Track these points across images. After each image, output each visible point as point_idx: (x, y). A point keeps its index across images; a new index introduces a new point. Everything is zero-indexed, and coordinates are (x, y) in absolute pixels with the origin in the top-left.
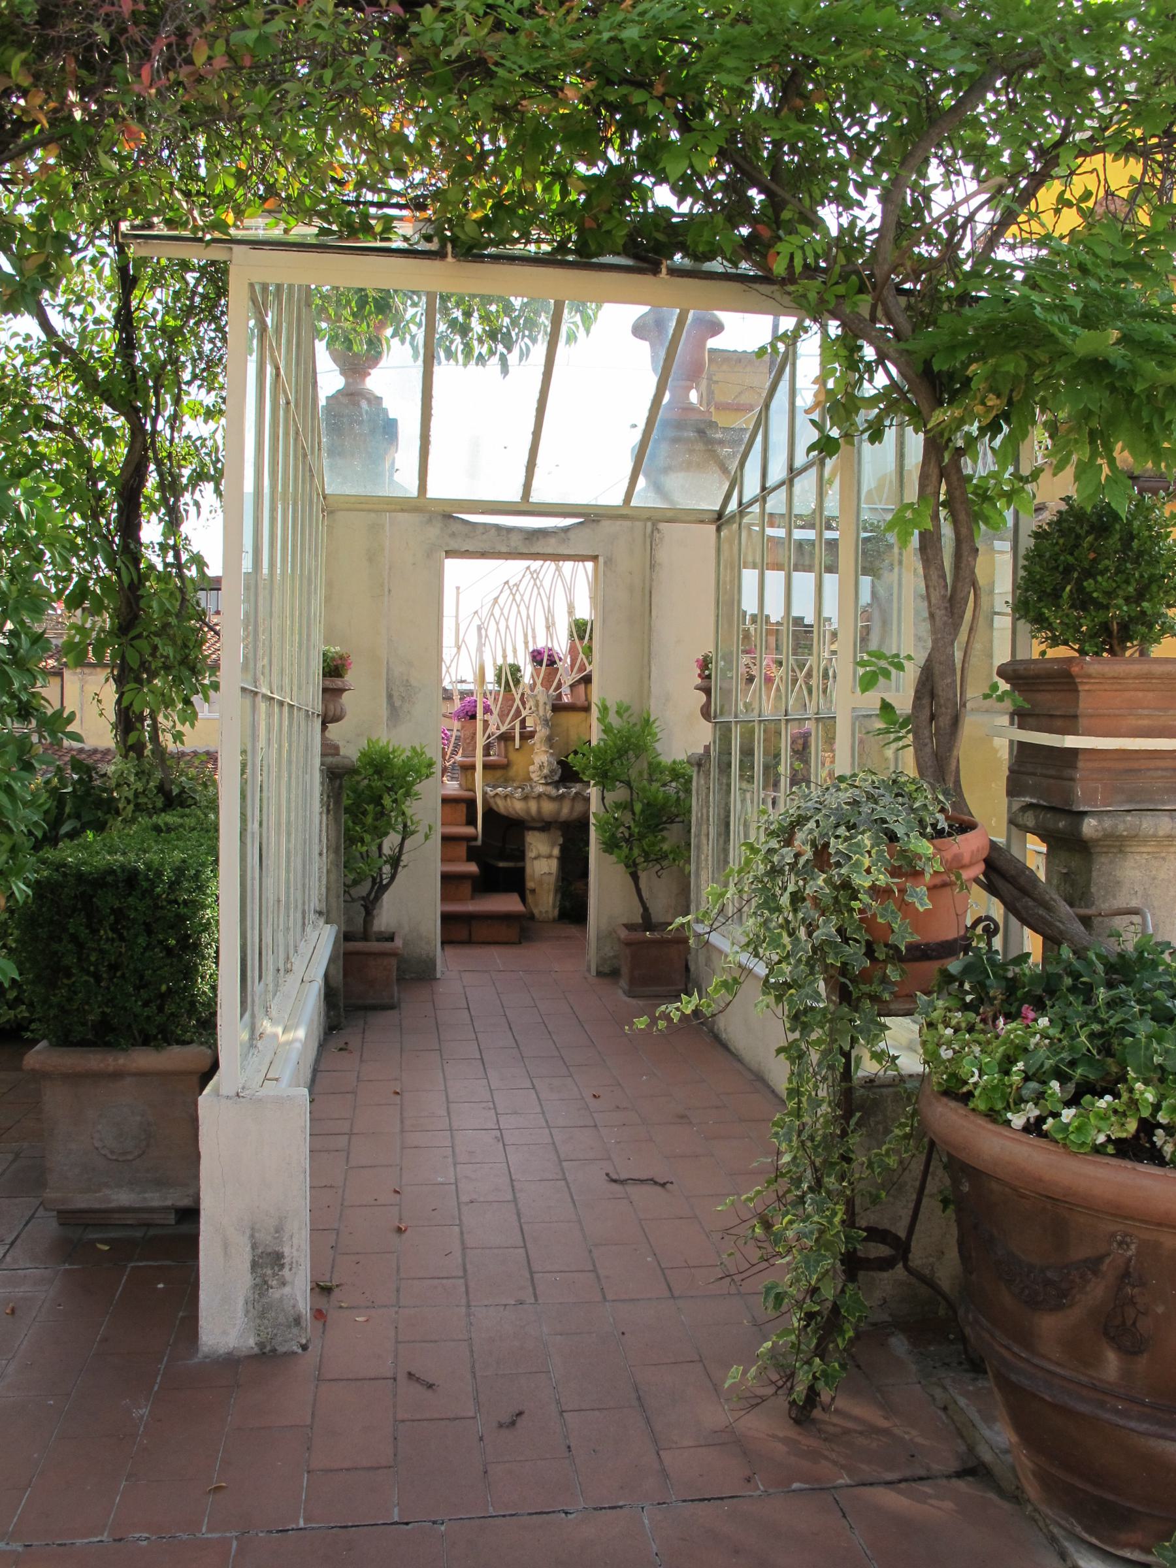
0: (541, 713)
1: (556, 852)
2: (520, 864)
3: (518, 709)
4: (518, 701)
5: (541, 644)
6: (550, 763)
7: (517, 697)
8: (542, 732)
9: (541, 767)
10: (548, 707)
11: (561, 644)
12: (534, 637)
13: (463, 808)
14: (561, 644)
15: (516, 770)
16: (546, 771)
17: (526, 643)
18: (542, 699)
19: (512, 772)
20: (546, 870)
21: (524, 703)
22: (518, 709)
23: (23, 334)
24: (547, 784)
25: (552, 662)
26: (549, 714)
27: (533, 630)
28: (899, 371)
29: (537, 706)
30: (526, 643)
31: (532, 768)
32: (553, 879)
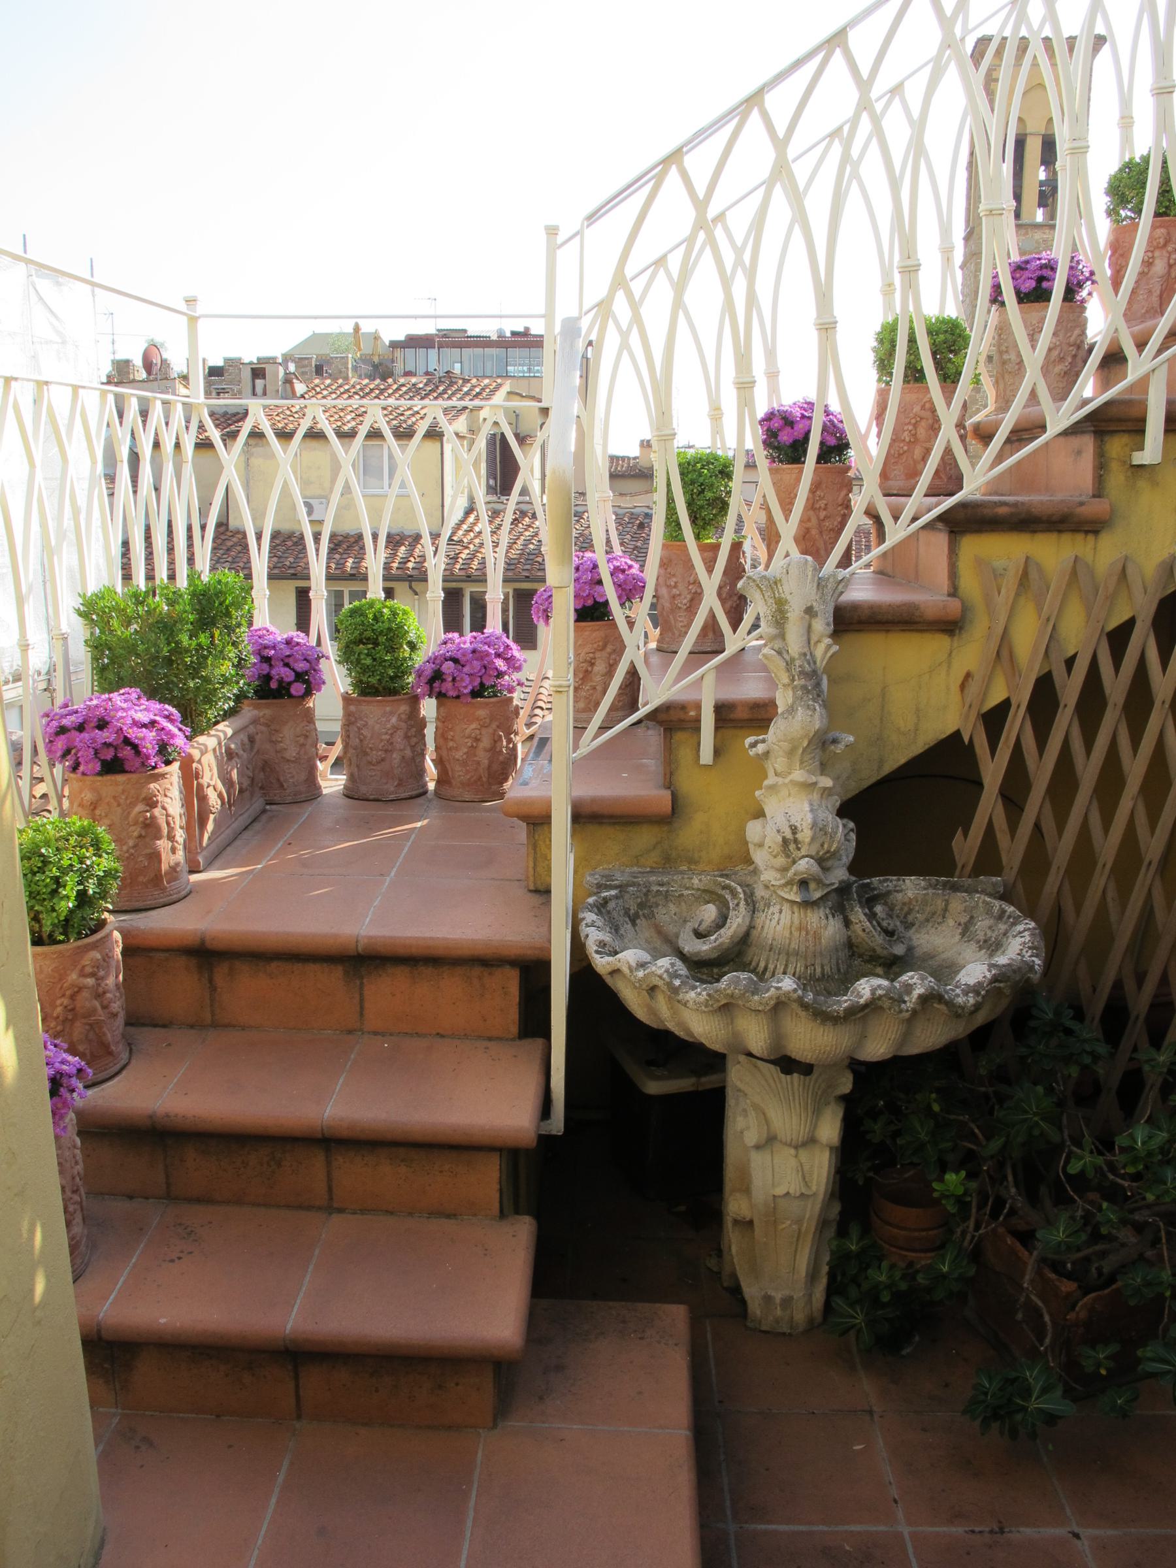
0: (795, 643)
1: (830, 1129)
2: (708, 1081)
3: (949, 463)
4: (711, 601)
5: (795, 390)
6: (819, 829)
7: (711, 583)
8: (795, 722)
9: (789, 844)
10: (822, 625)
11: (858, 398)
12: (773, 375)
13: (507, 989)
14: (858, 398)
15: (704, 827)
16: (804, 865)
17: (745, 387)
18: (798, 593)
19: (688, 835)
20: (789, 1183)
21: (736, 608)
22: (711, 626)
23: (543, 405)
24: (807, 904)
25: (835, 447)
26: (824, 649)
27: (771, 354)
28: (43, 1246)
29: (780, 619)
30: (745, 387)
31: (754, 830)
32: (812, 1210)
